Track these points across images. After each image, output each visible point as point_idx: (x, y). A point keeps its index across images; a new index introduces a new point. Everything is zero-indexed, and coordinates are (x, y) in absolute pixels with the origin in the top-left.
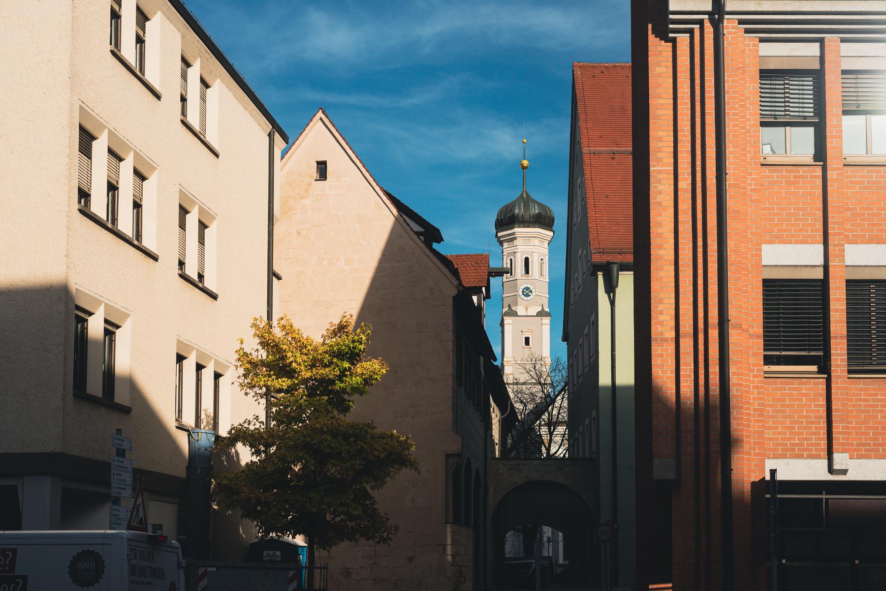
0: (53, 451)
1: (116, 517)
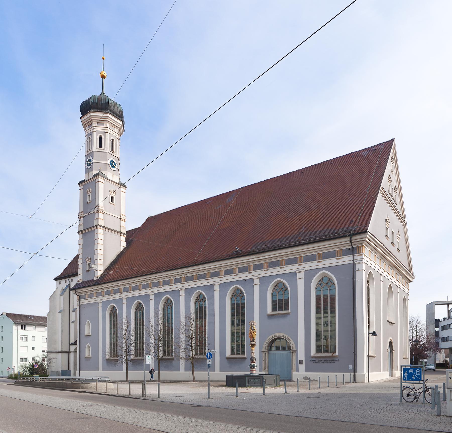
0: (17, 392)
1: (121, 356)
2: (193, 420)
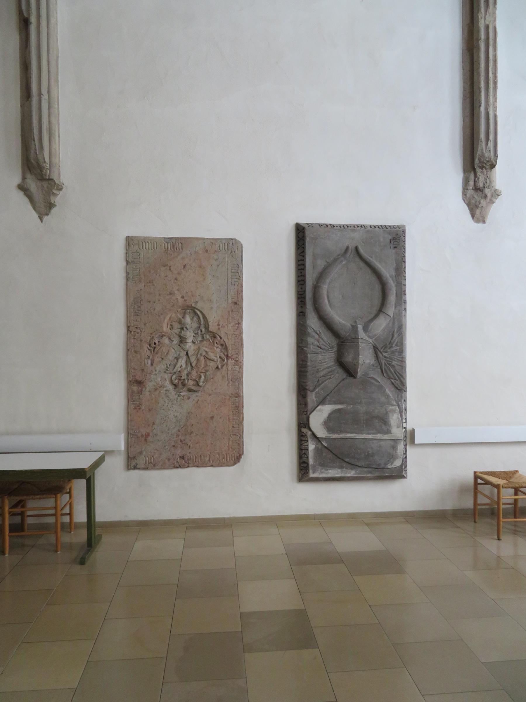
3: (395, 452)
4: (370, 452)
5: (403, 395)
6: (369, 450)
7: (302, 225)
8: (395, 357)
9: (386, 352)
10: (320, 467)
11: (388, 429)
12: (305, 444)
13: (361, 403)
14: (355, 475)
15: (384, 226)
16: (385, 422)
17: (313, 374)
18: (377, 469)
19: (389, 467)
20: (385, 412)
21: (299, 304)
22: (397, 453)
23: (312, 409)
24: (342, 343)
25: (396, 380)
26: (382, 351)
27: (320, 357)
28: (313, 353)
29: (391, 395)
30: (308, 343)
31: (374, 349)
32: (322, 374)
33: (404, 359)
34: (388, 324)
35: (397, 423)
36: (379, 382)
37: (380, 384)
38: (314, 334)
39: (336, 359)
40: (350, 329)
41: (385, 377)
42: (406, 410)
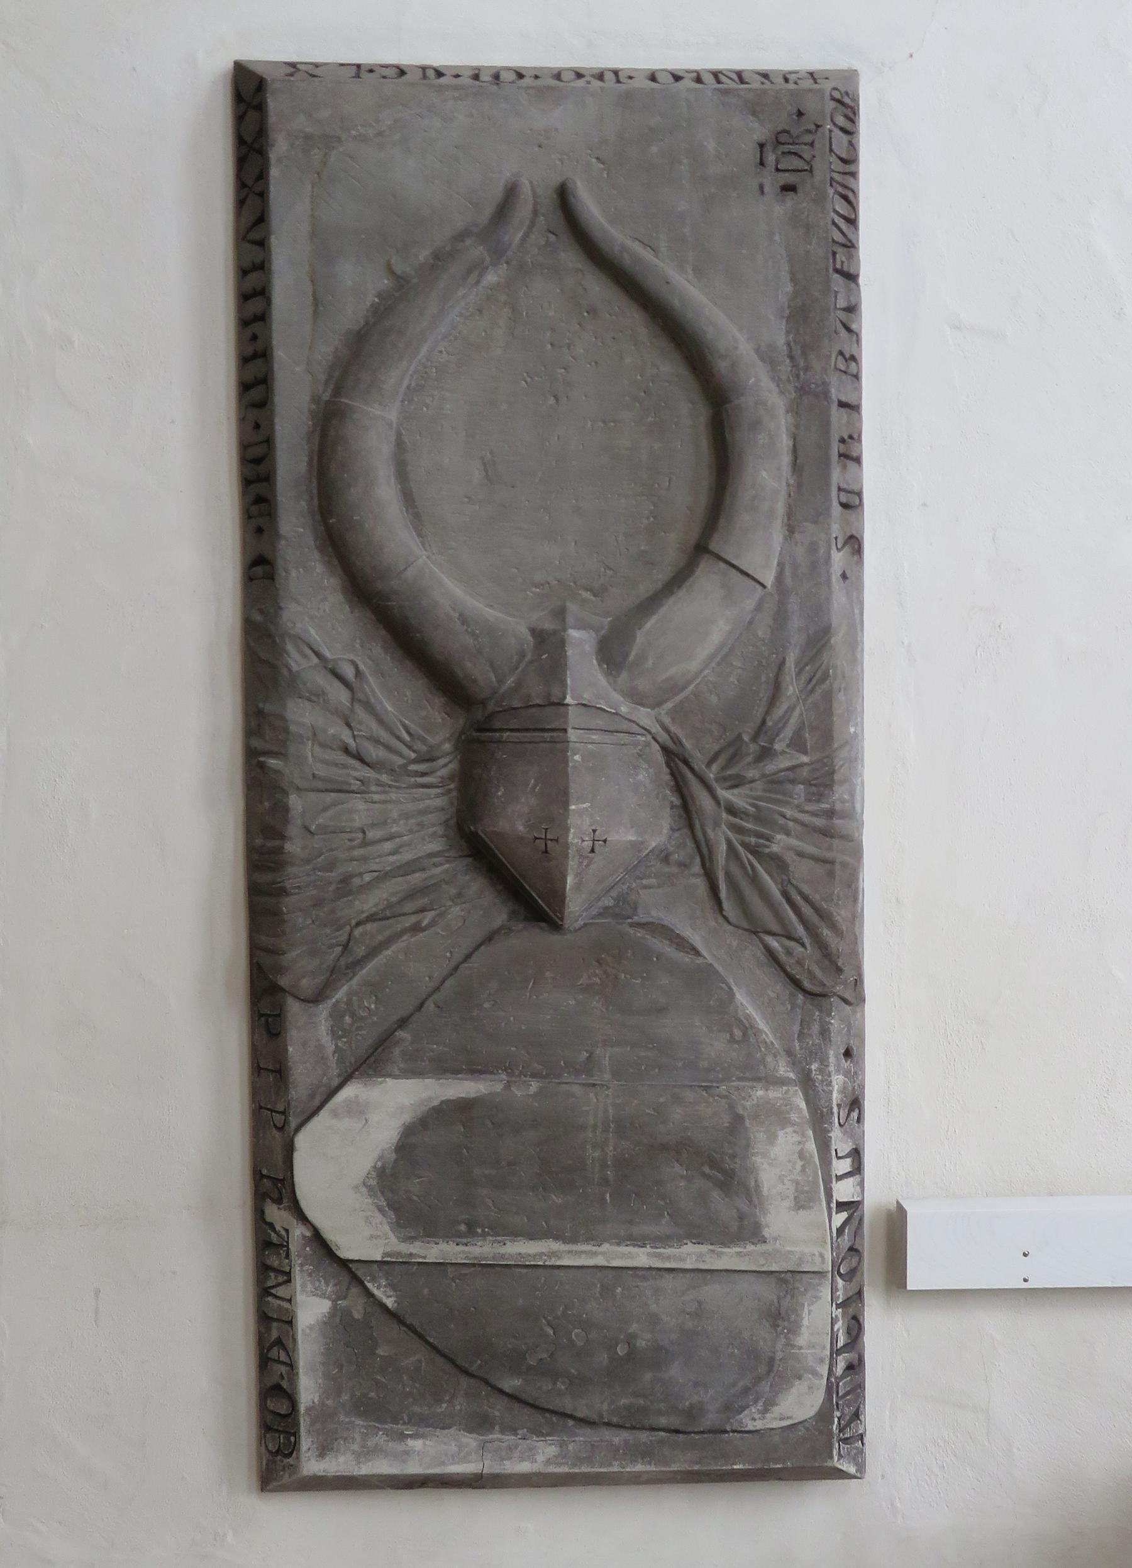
2: (279, 499)
3: (783, 1340)
4: (641, 1343)
5: (835, 1023)
6: (634, 1328)
7: (252, 67)
8: (789, 813)
9: (737, 782)
10: (359, 1422)
11: (741, 1217)
12: (281, 1291)
13: (590, 1066)
14: (559, 1464)
15: (735, 77)
16: (730, 1175)
17: (318, 903)
18: (681, 1437)
19: (750, 1427)
20: (726, 1121)
21: (250, 517)
22: (793, 1346)
23: (312, 1096)
24: (479, 730)
25: (790, 938)
26: (711, 775)
27: (359, 811)
28: (319, 791)
29: (762, 1024)
30: (286, 730)
31: (668, 765)
32: (370, 902)
33: (837, 821)
34: (750, 623)
35: (797, 1183)
36: (697, 953)
37: (699, 961)
38: (322, 680)
39: (453, 822)
40: (522, 655)
41: (726, 918)
42: (855, 1104)
